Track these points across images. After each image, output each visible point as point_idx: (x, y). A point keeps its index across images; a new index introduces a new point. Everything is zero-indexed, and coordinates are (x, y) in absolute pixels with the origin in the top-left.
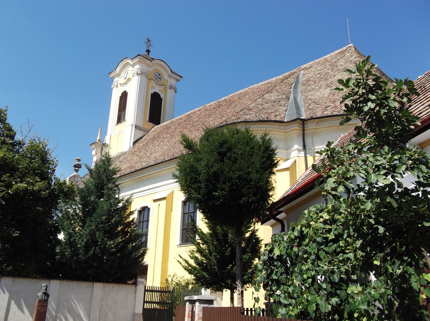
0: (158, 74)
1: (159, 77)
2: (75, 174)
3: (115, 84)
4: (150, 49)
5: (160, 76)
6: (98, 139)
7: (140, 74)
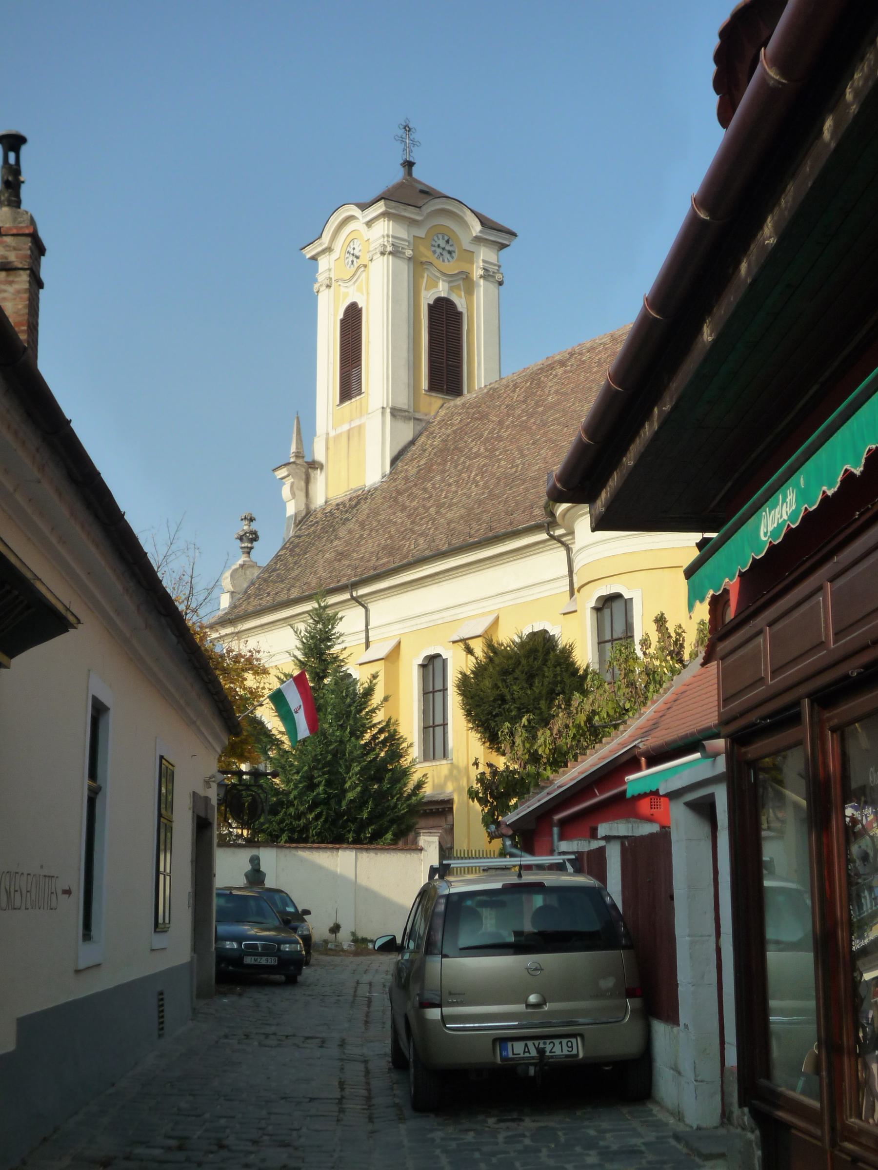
0: (443, 238)
1: (448, 248)
2: (244, 561)
3: (321, 278)
4: (415, 157)
5: (451, 242)
6: (292, 451)
7: (390, 253)
